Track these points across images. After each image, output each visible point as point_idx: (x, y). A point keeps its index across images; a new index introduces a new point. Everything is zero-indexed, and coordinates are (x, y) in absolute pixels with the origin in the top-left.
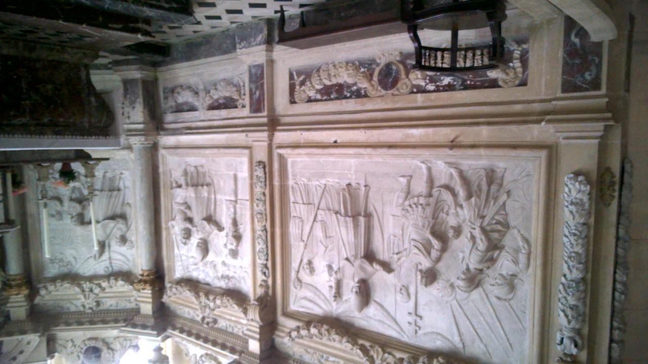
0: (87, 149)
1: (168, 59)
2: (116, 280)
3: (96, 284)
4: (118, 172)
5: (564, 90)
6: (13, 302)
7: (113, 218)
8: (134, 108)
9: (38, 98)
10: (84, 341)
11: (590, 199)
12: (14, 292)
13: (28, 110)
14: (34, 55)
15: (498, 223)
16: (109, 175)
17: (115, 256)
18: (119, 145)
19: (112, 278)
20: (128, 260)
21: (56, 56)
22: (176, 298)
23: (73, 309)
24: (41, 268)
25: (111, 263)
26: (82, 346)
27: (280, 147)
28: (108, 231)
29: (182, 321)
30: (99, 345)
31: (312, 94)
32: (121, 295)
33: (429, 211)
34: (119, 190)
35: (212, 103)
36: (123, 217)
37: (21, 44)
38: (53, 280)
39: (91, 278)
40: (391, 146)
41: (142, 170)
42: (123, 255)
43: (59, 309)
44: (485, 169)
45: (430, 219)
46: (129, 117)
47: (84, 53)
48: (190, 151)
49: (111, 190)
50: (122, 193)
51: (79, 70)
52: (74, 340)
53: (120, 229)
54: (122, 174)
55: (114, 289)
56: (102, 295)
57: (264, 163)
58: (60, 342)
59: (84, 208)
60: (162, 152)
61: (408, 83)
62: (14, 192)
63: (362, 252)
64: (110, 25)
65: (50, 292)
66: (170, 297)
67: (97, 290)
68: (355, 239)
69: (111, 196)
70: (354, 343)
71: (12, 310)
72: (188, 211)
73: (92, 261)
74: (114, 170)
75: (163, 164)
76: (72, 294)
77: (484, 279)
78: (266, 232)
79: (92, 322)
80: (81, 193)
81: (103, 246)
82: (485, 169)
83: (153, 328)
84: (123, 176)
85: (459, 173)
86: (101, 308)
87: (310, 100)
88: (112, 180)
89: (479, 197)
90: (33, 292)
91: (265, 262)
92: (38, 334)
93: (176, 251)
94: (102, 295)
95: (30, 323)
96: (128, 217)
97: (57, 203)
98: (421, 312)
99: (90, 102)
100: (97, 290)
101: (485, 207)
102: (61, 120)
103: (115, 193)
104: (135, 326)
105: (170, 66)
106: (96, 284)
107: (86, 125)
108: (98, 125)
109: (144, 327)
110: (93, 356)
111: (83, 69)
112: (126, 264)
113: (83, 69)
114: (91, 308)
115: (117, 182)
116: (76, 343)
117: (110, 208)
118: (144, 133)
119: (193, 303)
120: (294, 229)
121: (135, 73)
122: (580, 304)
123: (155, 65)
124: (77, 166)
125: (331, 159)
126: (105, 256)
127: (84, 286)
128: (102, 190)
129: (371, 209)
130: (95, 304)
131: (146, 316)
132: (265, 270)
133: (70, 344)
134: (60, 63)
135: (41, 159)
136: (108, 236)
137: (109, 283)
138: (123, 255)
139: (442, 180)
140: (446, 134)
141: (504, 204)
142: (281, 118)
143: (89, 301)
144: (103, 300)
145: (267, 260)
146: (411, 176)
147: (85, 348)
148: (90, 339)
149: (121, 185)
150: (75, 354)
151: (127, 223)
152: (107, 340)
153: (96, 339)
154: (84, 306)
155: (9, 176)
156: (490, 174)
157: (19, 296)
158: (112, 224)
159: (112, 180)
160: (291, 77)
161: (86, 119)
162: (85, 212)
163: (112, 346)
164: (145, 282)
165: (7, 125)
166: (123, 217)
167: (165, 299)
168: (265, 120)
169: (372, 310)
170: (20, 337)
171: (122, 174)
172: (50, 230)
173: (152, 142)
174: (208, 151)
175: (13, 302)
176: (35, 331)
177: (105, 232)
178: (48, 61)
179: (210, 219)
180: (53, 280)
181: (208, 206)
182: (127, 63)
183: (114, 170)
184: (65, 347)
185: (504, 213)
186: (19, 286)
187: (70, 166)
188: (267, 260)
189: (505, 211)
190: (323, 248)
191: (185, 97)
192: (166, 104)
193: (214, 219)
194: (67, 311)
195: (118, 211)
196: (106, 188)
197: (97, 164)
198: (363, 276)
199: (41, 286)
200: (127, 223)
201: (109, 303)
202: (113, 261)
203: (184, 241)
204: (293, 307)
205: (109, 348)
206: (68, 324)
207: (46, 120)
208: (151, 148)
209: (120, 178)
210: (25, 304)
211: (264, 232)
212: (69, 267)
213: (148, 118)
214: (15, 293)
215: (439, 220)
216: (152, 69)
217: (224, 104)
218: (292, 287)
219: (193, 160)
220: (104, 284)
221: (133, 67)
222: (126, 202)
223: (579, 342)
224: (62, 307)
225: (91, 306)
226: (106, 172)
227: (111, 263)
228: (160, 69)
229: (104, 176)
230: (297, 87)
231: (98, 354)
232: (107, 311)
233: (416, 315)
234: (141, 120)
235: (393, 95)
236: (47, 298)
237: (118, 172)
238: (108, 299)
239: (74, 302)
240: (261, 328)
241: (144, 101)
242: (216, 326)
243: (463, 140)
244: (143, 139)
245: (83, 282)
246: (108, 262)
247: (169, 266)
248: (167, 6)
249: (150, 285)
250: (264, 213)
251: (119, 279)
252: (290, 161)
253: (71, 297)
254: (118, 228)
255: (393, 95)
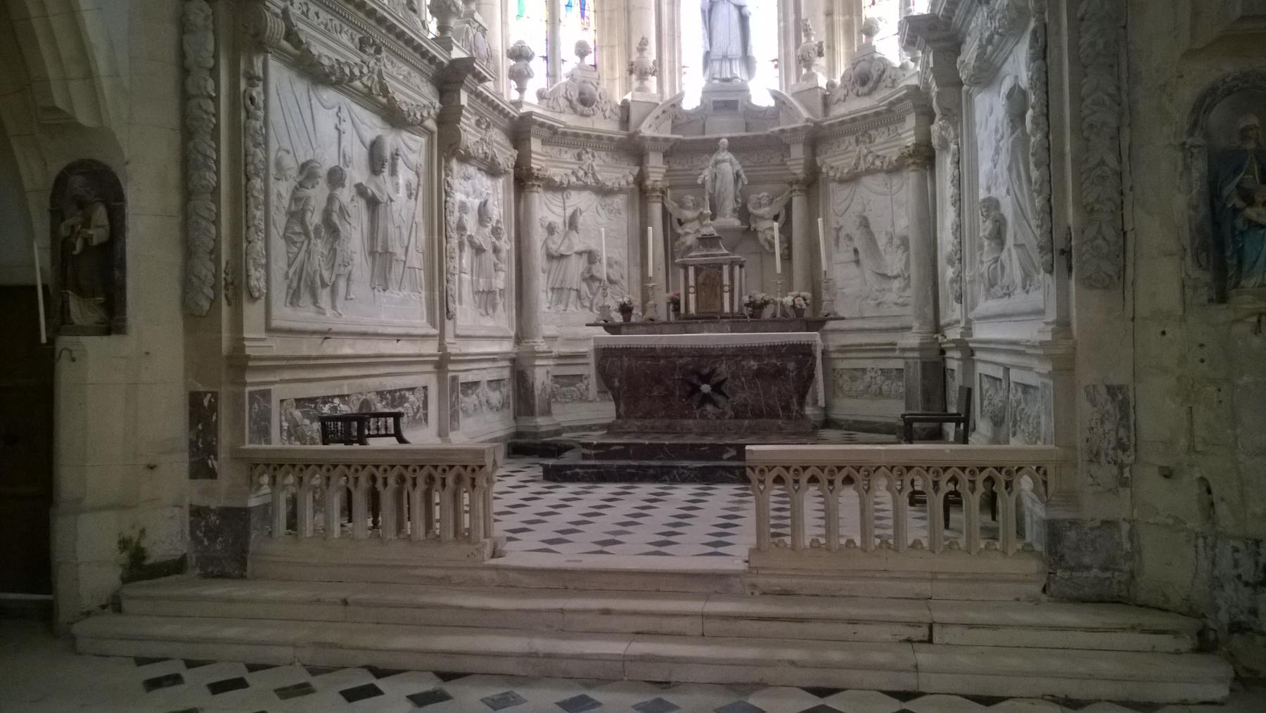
0: (608, 335)
1: (509, 441)
2: (562, 183)
3: (581, 180)
4: (553, 310)
5: (269, 392)
6: (660, 173)
7: (562, 256)
8: (543, 384)
9: (668, 382)
10: (594, 115)
11: (247, 270)
12: (659, 185)
13: (677, 370)
14: (667, 421)
15: (294, 243)
16: (562, 307)
17: (559, 211)
18: (595, 338)
19: (565, 186)
20: (546, 204)
21: (647, 422)
22: (506, 156)
23: (603, 154)
24: (630, 203)
25: (564, 203)
26: (596, 109)
27: (434, 336)
28: (567, 241)
29: (502, 125)
30: (580, 107)
31: (412, 398)
32: (555, 164)
33: (339, 260)
34: (553, 289)
35: (476, 389)
36: (551, 257)
37: (679, 429)
38: (621, 191)
39: (585, 187)
40: (364, 335)
41: (536, 312)
42: (553, 213)
43: (616, 156)
44: (298, 306)
45: (339, 249)
46: (548, 372)
47: (622, 428)
48: (492, 334)
49: (562, 289)
50: (550, 285)
51: (626, 412)
52: (603, 118)
53: (554, 243)
54: (549, 308)
55: (562, 171)
56: (576, 167)
57: (448, 318)
58: (616, 118)
59: (589, 270)
60: (512, 333)
61: (352, 406)
62: (679, 295)
63: (381, 208)
64: (622, 447)
65: (624, 177)
66: (512, 156)
67: (581, 173)
68: (387, 227)
69: (562, 281)
70: (392, 100)
71: (661, 165)
72: (497, 261)
73: (583, 207)
74: (557, 312)
75: (512, 318)
76: (604, 172)
77: (297, 176)
78: (446, 236)
79: (588, 136)
80: (589, 287)
81: (572, 223)
82: (298, 306)
83: (535, 122)
84: (548, 305)
85: (317, 302)
86: (576, 151)
87: (412, 389)
88: (559, 301)
89: (308, 273)
90: (640, 180)
91: (448, 199)
92: (641, 135)
93: (502, 211)
94: (576, 167)
95: (824, 170)
96: (545, 257)
97: (612, 277)
98: (335, 133)
99: (620, 382)
100: (581, 173)
101: (304, 262)
102: (649, 362)
103: (557, 286)
104: (551, 127)
105: (507, 432)
106: (581, 180)
107: (625, 359)
108: (614, 359)
109: (542, 125)
110: (587, 96)
111: (623, 414)
112: (549, 201)
113: (623, 414)
114: (587, 152)
115: (554, 299)
116: (602, 114)
117: (563, 267)
118: (535, 355)
119: (498, 149)
120: (422, 236)
121: (542, 422)
122: (252, 149)
123: (518, 434)
124: (618, 318)
125: (397, 321)
126: (569, 211)
127: (592, 181)
128: (570, 289)
129: (370, 260)
130: (583, 157)
131: (537, 136)
132: (448, 189)
133: (607, 114)
134: (644, 417)
135: (651, 325)
136: (566, 235)
137: (569, 181)
138: (553, 213)
139: (326, 291)
140: (331, 348)
141: (289, 266)
142: (433, 370)
143: (589, 162)
144: (573, 160)
145: (446, 202)
146: (346, 299)
147: (594, 106)
148: (587, 116)
149: (550, 294)
150: (603, 102)
151: (547, 249)
152: (572, 111)
153: (583, 115)
154: (593, 156)
155: (682, 310)
156: (294, 300)
157: (654, 179)
158: (563, 250)
159: (559, 301)
160: (426, 420)
161: (626, 364)
162: (586, 265)
163: (567, 103)
164: (537, 178)
165: (694, 356)
166: (551, 257)
167: (515, 153)
168: (451, 367)
169: (369, 136)
170: (656, 134)
171: (549, 308)
172: (602, 246)
173: (523, 344)
174: (483, 333)
175: (660, 173)
176: (644, 138)
177: (570, 239)
178: (653, 417)
179: (479, 250)
180: (621, 191)
181: (480, 264)
182: (548, 434)
183: (557, 312)
184: (612, 110)
185: (290, 255)
186: (654, 190)
187: (624, 318)
188: (446, 202)
189: (288, 257)
190: (403, 214)
191: (495, 397)
192: (507, 390)
193: (474, 251)
194: (609, 153)
195: (555, 264)
196: (566, 292)
197: (598, 319)
198: (376, 179)
199: (632, 186)
200: (547, 249)
201: (568, 156)
202: (561, 205)
203: (500, 225)
204: (422, 140)
205: (570, 102)
206: (611, 139)
207: (662, 362)
208: (523, 338)
209: (551, 303)
210: (650, 170)
211: (448, 236)
212: (603, 204)
213: (528, 372)
214: (659, 183)
215: (329, 246)
216: (521, 429)
217: (469, 388)
218: (423, 164)
219: (488, 322)
220: (573, 179)
221: (544, 429)
222: (546, 274)
223: (249, 102)
224: (613, 157)
225: (587, 156)
226: (565, 310)
227: (564, 203)
228: (513, 430)
229: (567, 306)
230: (421, 405)
231: (582, 96)
232: (570, 146)
233: (339, 130)
234: (537, 370)
235: (361, 393)
236: (627, 172)
237: (553, 310)
238: (568, 160)
239: (602, 163)
240: (458, 121)
241: (533, 391)
242: (478, 118)
243: (317, 340)
244: (536, 348)
245: (594, 184)
246: (567, 204)
247: (509, 193)
248: (577, 470)
249: (533, 174)
250: (448, 259)
251: (559, 183)
252: (425, 321)
253: (606, 169)
254: (557, 245)
255: (361, 393)
